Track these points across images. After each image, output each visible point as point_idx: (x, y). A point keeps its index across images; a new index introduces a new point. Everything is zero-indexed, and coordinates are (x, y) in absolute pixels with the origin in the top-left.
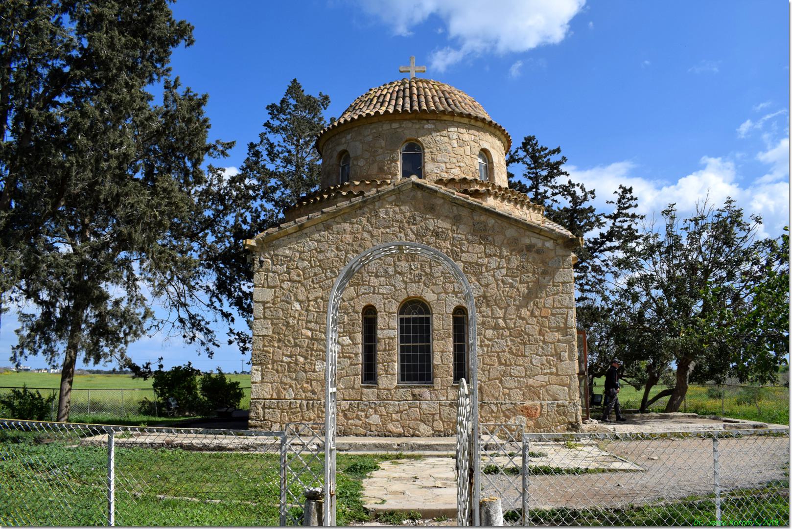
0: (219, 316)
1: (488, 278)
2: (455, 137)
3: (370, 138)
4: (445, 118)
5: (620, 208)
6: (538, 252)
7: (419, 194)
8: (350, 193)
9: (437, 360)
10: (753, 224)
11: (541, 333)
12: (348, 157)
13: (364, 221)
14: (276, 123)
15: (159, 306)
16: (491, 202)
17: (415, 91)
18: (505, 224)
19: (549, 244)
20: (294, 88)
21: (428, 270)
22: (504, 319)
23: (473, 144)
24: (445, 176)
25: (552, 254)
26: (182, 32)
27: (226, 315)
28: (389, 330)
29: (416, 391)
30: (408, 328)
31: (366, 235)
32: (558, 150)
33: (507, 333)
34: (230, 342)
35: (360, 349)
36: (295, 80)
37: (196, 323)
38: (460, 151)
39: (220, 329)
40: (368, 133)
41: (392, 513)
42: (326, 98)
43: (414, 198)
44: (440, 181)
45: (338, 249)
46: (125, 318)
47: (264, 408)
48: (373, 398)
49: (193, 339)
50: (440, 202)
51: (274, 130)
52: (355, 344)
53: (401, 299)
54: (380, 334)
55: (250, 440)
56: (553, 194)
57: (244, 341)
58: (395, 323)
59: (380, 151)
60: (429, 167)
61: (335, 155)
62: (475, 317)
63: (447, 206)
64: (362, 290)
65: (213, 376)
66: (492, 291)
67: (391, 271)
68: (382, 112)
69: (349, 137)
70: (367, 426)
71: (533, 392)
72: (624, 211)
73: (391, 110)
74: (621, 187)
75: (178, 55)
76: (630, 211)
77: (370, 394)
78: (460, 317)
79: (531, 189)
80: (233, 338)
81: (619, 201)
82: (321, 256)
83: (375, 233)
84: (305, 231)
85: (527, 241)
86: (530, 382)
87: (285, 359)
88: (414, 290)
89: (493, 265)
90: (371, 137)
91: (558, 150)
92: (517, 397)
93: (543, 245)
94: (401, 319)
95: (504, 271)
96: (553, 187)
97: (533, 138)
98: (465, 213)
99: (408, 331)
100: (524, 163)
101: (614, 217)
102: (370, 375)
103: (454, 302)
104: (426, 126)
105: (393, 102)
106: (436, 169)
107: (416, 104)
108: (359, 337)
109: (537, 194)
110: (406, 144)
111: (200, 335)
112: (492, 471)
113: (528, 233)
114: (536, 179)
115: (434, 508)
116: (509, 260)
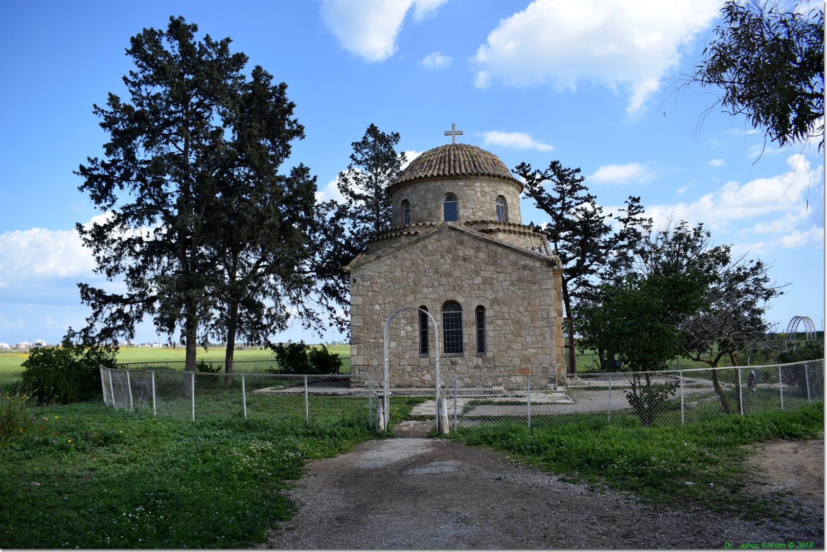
0: (325, 310)
1: (497, 287)
5: (630, 214)
6: (530, 270)
7: (453, 233)
8: (409, 233)
9: (465, 340)
10: (705, 236)
11: (532, 321)
12: (408, 203)
13: (418, 251)
14: (359, 156)
15: (293, 310)
16: (501, 237)
17: (452, 158)
18: (509, 252)
19: (538, 264)
20: (372, 130)
21: (459, 282)
22: (509, 313)
24: (472, 218)
26: (299, 132)
27: (330, 309)
28: (436, 323)
29: (453, 359)
30: (448, 320)
31: (419, 261)
32: (578, 170)
33: (510, 322)
34: (331, 325)
35: (417, 334)
37: (309, 314)
38: (483, 199)
39: (324, 316)
40: (421, 187)
41: (422, 417)
42: (397, 135)
43: (450, 236)
44: (467, 223)
45: (402, 271)
47: (359, 371)
48: (427, 364)
49: (309, 326)
51: (359, 163)
52: (415, 330)
55: (352, 390)
56: (577, 204)
57: (341, 323)
58: (440, 316)
60: (461, 212)
61: (400, 202)
63: (471, 241)
64: (418, 296)
65: (319, 350)
66: (500, 295)
67: (436, 284)
68: (429, 175)
70: (423, 381)
71: (527, 359)
72: (633, 217)
73: (435, 174)
74: (630, 197)
75: (295, 143)
76: (638, 217)
77: (424, 361)
78: (480, 310)
79: (559, 200)
80: (333, 321)
81: (630, 208)
82: (391, 275)
83: (426, 259)
85: (523, 263)
86: (525, 353)
87: (371, 341)
88: (451, 296)
89: (501, 279)
91: (578, 170)
92: (517, 362)
95: (508, 283)
96: (577, 198)
97: (558, 162)
98: (483, 244)
100: (553, 180)
101: (625, 221)
102: (425, 349)
103: (475, 304)
105: (437, 167)
106: (465, 213)
107: (452, 168)
108: (417, 326)
109: (564, 204)
111: (313, 323)
114: (562, 192)
116: (511, 274)
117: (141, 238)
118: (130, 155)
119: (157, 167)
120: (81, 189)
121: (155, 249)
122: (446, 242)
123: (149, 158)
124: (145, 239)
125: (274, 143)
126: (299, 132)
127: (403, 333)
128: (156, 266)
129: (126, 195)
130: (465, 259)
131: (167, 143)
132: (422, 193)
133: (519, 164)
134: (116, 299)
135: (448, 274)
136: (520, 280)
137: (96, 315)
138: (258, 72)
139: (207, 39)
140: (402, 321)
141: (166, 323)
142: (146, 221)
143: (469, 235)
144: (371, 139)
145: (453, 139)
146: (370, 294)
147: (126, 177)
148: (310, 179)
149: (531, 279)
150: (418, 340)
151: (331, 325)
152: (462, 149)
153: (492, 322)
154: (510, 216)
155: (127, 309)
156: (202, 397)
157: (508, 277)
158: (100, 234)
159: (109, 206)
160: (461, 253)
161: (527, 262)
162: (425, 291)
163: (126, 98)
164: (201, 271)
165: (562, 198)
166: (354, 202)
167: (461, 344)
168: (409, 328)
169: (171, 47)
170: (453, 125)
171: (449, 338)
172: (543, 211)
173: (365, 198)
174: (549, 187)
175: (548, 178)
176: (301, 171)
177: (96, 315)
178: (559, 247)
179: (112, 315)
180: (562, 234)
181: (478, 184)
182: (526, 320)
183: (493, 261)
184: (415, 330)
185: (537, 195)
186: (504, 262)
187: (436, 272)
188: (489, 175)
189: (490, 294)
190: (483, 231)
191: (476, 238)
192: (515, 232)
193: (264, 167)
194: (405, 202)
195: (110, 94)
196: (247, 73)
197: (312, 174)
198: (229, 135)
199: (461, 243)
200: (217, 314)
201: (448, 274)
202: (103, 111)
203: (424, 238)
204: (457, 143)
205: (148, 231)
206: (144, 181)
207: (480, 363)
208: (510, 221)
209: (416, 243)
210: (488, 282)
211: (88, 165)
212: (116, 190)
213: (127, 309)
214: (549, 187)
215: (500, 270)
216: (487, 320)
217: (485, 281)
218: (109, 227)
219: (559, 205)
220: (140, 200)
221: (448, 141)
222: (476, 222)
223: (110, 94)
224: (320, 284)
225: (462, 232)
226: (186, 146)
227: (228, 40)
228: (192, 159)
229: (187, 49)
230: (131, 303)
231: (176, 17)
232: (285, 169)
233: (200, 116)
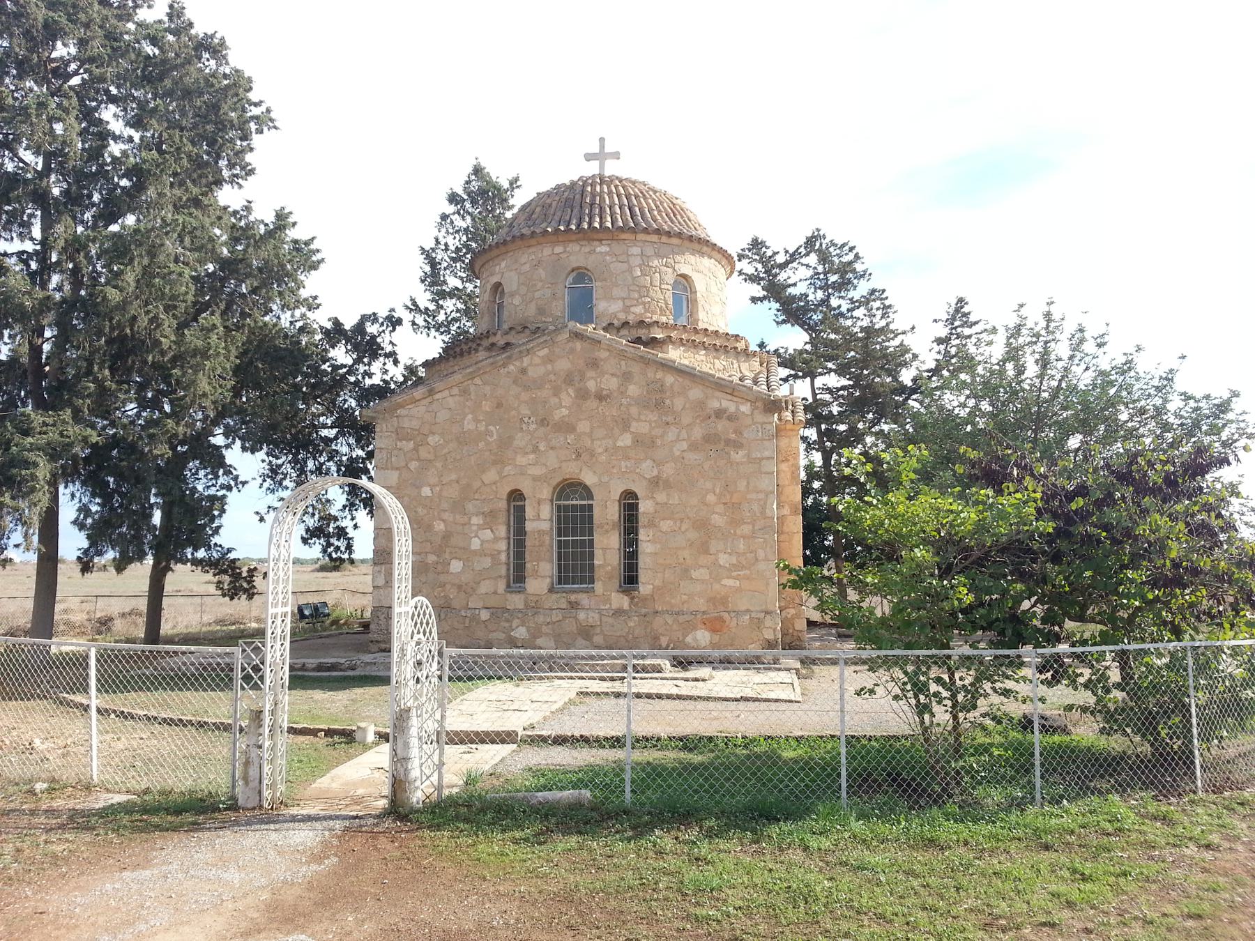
2: (638, 261)
3: (527, 267)
4: (624, 236)
6: (730, 418)
7: (578, 345)
16: (675, 354)
18: (687, 382)
19: (745, 408)
25: (749, 421)
26: (265, 121)
28: (541, 519)
29: (573, 597)
36: (478, 171)
43: (572, 351)
48: (521, 606)
50: (604, 354)
53: (554, 482)
54: (529, 526)
58: (546, 511)
62: (644, 507)
66: (669, 470)
77: (516, 601)
85: (715, 404)
88: (572, 470)
93: (737, 409)
94: (559, 507)
95: (685, 445)
98: (636, 368)
103: (617, 490)
104: (598, 249)
108: (502, 530)
110: (574, 274)
113: (718, 394)
115: (375, 688)
122: (563, 365)
126: (265, 121)
127: (475, 544)
130: (600, 397)
135: (566, 427)
136: (710, 439)
140: (475, 520)
143: (609, 349)
145: (602, 167)
150: (503, 557)
154: (701, 315)
156: (293, 692)
160: (591, 385)
161: (725, 404)
162: (521, 460)
168: (488, 534)
170: (602, 140)
181: (636, 250)
182: (718, 520)
185: (775, 291)
186: (679, 403)
188: (658, 231)
189: (648, 469)
191: (622, 355)
199: (594, 364)
201: (566, 427)
204: (607, 173)
207: (626, 606)
208: (701, 326)
210: (644, 443)
214: (799, 280)
216: (642, 520)
221: (592, 169)
222: (626, 324)
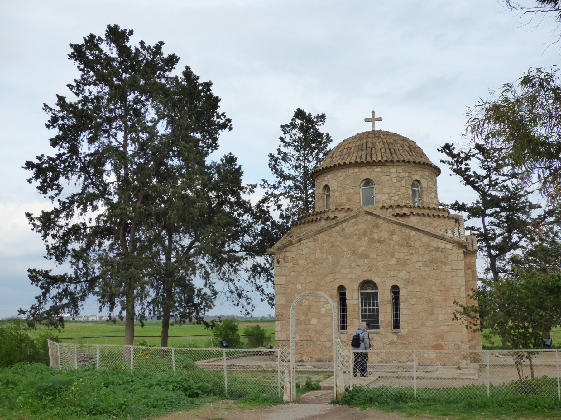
7: (369, 217)
15: (219, 286)
18: (421, 234)
19: (449, 246)
23: (407, 178)
28: (354, 300)
34: (262, 300)
45: (321, 252)
46: (203, 297)
59: (348, 187)
61: (322, 187)
64: (338, 276)
69: (329, 176)
75: (223, 135)
78: (395, 290)
80: (264, 297)
84: (302, 242)
85: (435, 245)
88: (368, 276)
90: (342, 177)
94: (361, 293)
95: (421, 264)
98: (396, 227)
99: (365, 300)
104: (376, 170)
105: (355, 155)
109: (490, 181)
110: (364, 182)
112: (361, 364)
114: (488, 169)
117: (84, 224)
118: (74, 150)
119: (96, 163)
120: (29, 181)
121: (100, 232)
122: (362, 226)
123: (92, 151)
124: (88, 225)
125: (204, 136)
128: (97, 248)
129: (71, 185)
130: (380, 242)
131: (108, 137)
132: (341, 179)
133: (443, 145)
134: (62, 279)
135: (364, 256)
137: (44, 294)
138: (188, 73)
139: (142, 43)
141: (108, 298)
142: (89, 208)
143: (384, 219)
144: (298, 122)
145: (373, 126)
146: (293, 274)
147: (71, 168)
148: (237, 167)
149: (443, 260)
151: (262, 300)
152: (379, 137)
153: (406, 301)
155: (72, 287)
157: (420, 259)
158: (47, 221)
159: (56, 195)
160: (376, 236)
162: (344, 271)
163: (72, 98)
164: (140, 254)
165: (488, 176)
166: (283, 183)
167: (378, 321)
169: (110, 50)
171: (366, 315)
172: (469, 187)
173: (294, 178)
174: (475, 166)
175: (474, 156)
176: (230, 160)
177: (44, 294)
178: (486, 224)
179: (59, 293)
180: (489, 211)
181: (393, 170)
182: (437, 298)
183: (407, 243)
184: (334, 306)
186: (417, 244)
187: (354, 254)
189: (404, 275)
190: (398, 215)
191: (390, 221)
192: (428, 215)
193: (195, 156)
194: (326, 187)
195: (57, 96)
196: (178, 72)
197: (238, 162)
198: (162, 128)
199: (377, 226)
200: (152, 293)
201: (364, 256)
202: (51, 109)
203: (342, 222)
204: (377, 129)
205: (89, 217)
206: (87, 172)
207: (395, 339)
209: (334, 227)
210: (402, 263)
211: (36, 161)
212: (62, 180)
213: (72, 287)
215: (414, 252)
217: (399, 262)
218: (57, 213)
219: (486, 181)
220: (84, 189)
221: (368, 127)
223: (57, 96)
224: (249, 263)
225: (378, 216)
226: (125, 138)
227: (162, 43)
228: (131, 149)
229: (124, 50)
230: (76, 283)
231: (112, 25)
232: (214, 158)
233: (137, 113)
